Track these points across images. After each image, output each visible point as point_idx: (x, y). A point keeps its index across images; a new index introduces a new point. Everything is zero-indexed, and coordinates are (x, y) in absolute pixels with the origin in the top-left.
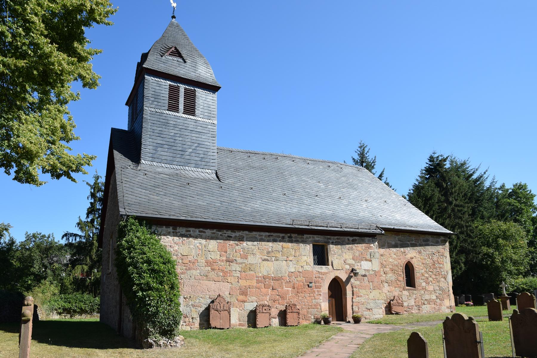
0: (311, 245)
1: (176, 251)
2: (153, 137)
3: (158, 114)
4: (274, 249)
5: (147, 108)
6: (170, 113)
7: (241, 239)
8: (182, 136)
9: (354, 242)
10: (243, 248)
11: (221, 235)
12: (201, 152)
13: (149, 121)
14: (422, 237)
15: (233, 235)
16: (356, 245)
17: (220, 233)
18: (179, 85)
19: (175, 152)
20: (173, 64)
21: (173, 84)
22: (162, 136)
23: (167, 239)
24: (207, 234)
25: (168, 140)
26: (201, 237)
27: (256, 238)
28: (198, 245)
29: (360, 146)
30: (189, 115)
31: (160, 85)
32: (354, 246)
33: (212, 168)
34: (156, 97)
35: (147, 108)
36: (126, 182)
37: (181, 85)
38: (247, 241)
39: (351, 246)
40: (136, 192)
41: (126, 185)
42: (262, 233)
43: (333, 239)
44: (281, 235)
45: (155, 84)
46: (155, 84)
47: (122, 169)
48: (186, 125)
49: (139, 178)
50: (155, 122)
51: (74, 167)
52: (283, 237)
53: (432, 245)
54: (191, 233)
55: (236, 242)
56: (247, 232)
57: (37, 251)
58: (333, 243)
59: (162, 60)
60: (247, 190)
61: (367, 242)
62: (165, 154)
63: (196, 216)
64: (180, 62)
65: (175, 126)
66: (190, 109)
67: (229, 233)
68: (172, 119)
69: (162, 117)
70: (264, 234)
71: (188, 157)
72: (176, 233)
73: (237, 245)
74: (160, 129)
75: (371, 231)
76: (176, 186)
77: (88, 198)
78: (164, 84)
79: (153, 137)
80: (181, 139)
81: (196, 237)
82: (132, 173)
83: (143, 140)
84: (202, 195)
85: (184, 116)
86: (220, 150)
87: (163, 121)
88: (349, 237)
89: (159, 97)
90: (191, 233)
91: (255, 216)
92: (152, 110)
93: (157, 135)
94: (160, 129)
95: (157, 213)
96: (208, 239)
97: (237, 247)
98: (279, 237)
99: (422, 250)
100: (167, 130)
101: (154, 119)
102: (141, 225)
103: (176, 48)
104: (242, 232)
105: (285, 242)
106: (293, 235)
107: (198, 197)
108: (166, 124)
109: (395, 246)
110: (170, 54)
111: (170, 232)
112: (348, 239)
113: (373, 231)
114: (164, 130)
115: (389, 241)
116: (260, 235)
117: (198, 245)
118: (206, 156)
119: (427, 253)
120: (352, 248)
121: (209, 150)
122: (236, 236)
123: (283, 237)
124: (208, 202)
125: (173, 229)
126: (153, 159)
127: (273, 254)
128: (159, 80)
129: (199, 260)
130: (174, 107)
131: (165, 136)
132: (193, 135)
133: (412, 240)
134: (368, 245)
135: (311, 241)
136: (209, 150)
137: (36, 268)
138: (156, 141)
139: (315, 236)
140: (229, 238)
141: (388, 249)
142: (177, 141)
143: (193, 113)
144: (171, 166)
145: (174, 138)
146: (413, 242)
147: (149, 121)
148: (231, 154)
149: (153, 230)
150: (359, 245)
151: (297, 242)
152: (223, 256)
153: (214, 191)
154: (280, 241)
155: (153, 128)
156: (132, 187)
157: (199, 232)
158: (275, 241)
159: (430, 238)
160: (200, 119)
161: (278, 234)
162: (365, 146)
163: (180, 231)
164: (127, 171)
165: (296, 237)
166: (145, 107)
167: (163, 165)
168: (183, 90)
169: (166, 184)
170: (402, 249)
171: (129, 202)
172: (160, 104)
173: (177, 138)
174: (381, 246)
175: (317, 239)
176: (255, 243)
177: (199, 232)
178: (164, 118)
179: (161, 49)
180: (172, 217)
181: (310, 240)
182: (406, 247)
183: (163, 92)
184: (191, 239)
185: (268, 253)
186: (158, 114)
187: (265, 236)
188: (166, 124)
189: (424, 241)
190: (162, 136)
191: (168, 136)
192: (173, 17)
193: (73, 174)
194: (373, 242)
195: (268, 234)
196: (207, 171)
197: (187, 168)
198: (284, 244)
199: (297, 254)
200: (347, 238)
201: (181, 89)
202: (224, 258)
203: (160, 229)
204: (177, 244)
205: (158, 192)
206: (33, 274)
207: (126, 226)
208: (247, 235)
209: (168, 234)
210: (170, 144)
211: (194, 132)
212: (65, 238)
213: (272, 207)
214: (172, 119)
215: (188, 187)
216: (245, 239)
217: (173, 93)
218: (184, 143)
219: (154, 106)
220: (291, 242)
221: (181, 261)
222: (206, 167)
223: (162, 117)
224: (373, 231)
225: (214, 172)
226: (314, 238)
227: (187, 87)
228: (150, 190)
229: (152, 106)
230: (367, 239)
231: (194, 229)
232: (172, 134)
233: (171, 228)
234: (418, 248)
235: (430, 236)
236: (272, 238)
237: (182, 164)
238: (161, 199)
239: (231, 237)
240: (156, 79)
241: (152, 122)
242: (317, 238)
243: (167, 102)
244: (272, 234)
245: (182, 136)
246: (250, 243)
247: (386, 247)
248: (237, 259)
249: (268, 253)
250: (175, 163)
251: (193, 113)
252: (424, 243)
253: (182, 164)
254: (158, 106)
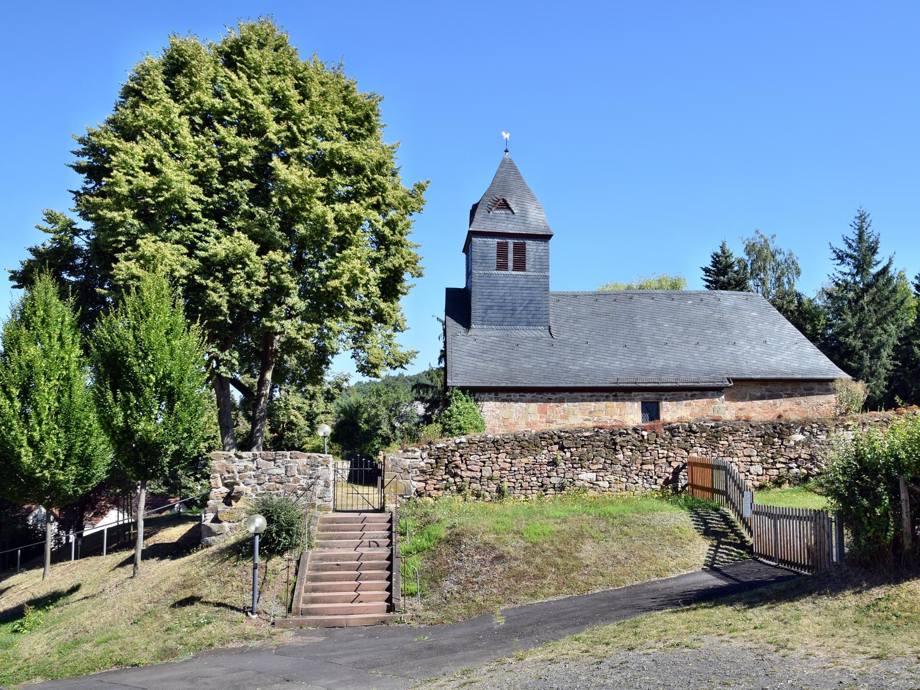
4: (596, 409)
5: (475, 272)
6: (499, 272)
7: (561, 401)
9: (693, 397)
10: (564, 410)
12: (532, 309)
14: (802, 386)
15: (554, 397)
16: (695, 400)
17: (540, 396)
19: (505, 312)
22: (491, 297)
25: (498, 301)
26: (522, 401)
32: (693, 402)
33: (545, 324)
35: (475, 272)
42: (584, 394)
44: (605, 394)
51: (404, 361)
53: (817, 394)
54: (512, 397)
56: (568, 394)
57: (384, 409)
58: (666, 400)
62: (496, 315)
65: (504, 285)
66: (520, 265)
67: (550, 395)
70: (585, 394)
71: (519, 316)
73: (558, 406)
74: (490, 291)
80: (511, 298)
81: (517, 401)
83: (472, 305)
85: (513, 273)
88: (687, 393)
90: (512, 397)
91: (579, 376)
92: (481, 272)
94: (490, 291)
99: (802, 401)
101: (482, 281)
102: (464, 394)
103: (504, 200)
105: (609, 401)
106: (619, 394)
107: (525, 359)
108: (495, 285)
109: (762, 398)
112: (686, 395)
116: (581, 396)
118: (537, 312)
120: (690, 405)
121: (541, 305)
123: (607, 397)
130: (502, 266)
131: (494, 297)
132: (523, 292)
133: (788, 390)
136: (541, 305)
137: (385, 429)
138: (485, 304)
139: (645, 393)
140: (549, 400)
146: (789, 392)
150: (699, 400)
151: (623, 400)
154: (604, 401)
155: (482, 291)
159: (816, 386)
160: (531, 274)
161: (602, 394)
162: (867, 214)
164: (458, 338)
165: (622, 396)
170: (771, 401)
173: (507, 298)
174: (727, 399)
183: (491, 251)
184: (512, 403)
185: (591, 412)
187: (587, 396)
189: (805, 390)
190: (491, 297)
191: (497, 297)
192: (506, 151)
194: (719, 396)
195: (590, 394)
198: (608, 403)
200: (684, 393)
201: (509, 245)
202: (544, 420)
203: (483, 396)
205: (485, 358)
206: (381, 436)
207: (451, 396)
209: (491, 400)
212: (415, 391)
213: (604, 363)
217: (502, 251)
218: (514, 301)
220: (617, 400)
222: (538, 324)
225: (547, 327)
229: (480, 268)
230: (710, 393)
232: (501, 294)
233: (493, 394)
235: (816, 384)
242: (647, 395)
243: (495, 261)
247: (747, 399)
250: (505, 323)
252: (805, 393)
254: (487, 268)
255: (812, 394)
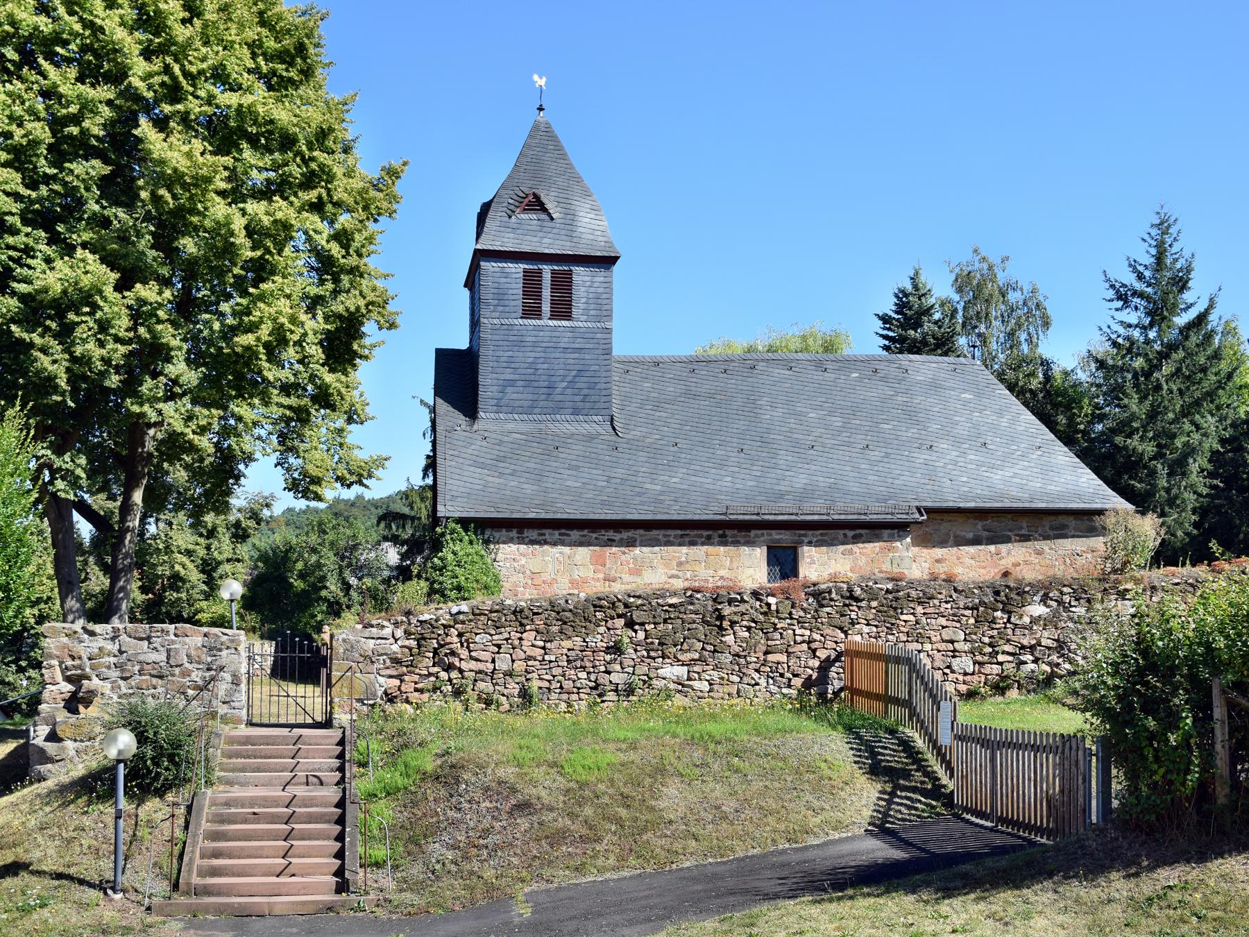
0: (765, 548)
1: (523, 566)
2: (498, 370)
3: (505, 327)
4: (690, 558)
5: (485, 321)
7: (631, 543)
8: (548, 361)
9: (856, 539)
10: (635, 559)
11: (596, 538)
13: (489, 342)
14: (1047, 522)
15: (617, 537)
16: (861, 545)
17: (594, 535)
18: (540, 267)
19: (537, 390)
20: (529, 227)
21: (531, 267)
23: (509, 549)
24: (573, 537)
25: (524, 371)
26: (563, 544)
27: (658, 540)
28: (557, 555)
29: (1158, 222)
30: (560, 320)
31: (507, 275)
32: (856, 548)
33: (603, 412)
34: (501, 297)
35: (485, 321)
36: (451, 458)
37: (545, 267)
38: (641, 545)
39: (849, 547)
40: (466, 473)
41: (451, 463)
42: (669, 532)
43: (813, 535)
44: (705, 533)
45: (499, 274)
46: (499, 274)
47: (448, 434)
48: (555, 339)
49: (473, 447)
50: (501, 343)
52: (709, 537)
53: (1073, 537)
55: (623, 549)
56: (641, 532)
58: (810, 543)
59: (510, 225)
60: (667, 448)
61: (885, 539)
62: (521, 396)
63: (554, 509)
64: (543, 220)
65: (535, 345)
66: (562, 309)
68: (529, 333)
69: (511, 333)
70: (672, 533)
71: (560, 398)
72: (523, 538)
73: (624, 553)
74: (510, 353)
75: (896, 518)
76: (535, 455)
77: (424, 434)
78: (514, 270)
79: (498, 370)
80: (546, 366)
81: (555, 544)
82: (463, 438)
83: (480, 378)
84: (577, 468)
85: (551, 323)
86: (634, 365)
87: (515, 338)
89: (506, 297)
91: (661, 502)
92: (495, 321)
93: (505, 365)
94: (510, 353)
95: (493, 510)
96: (575, 545)
97: (623, 557)
98: (701, 536)
99: (1046, 548)
100: (521, 354)
101: (497, 338)
102: (466, 530)
104: (633, 531)
106: (729, 532)
108: (519, 344)
109: (976, 541)
110: (525, 209)
111: (512, 538)
112: (845, 535)
113: (899, 516)
114: (517, 354)
115: (958, 533)
117: (557, 555)
118: (592, 392)
119: (1060, 552)
120: (851, 552)
122: (622, 539)
123: (709, 537)
124: (584, 480)
125: (518, 533)
126: (499, 408)
127: (688, 567)
128: (505, 265)
129: (559, 580)
130: (532, 311)
132: (568, 356)
133: (1021, 528)
134: (888, 544)
135: (764, 541)
136: (597, 380)
139: (773, 532)
140: (610, 543)
141: (955, 549)
142: (540, 372)
143: (567, 316)
144: (530, 416)
145: (534, 366)
146: (1023, 532)
147: (489, 342)
148: (657, 369)
149: (486, 537)
150: (866, 545)
151: (736, 543)
152: (599, 571)
153: (601, 457)
154: (703, 544)
155: (498, 354)
156: (460, 466)
157: (560, 534)
158: (692, 543)
159: (1071, 522)
160: (581, 324)
161: (700, 532)
163: (530, 535)
164: (456, 435)
165: (733, 536)
166: (482, 320)
167: (516, 416)
168: (549, 275)
169: (518, 452)
170: (992, 548)
171: (454, 493)
172: (507, 309)
173: (539, 366)
175: (778, 537)
176: (657, 549)
177: (560, 534)
178: (515, 333)
179: (511, 201)
180: (514, 516)
181: (762, 539)
182: (1003, 542)
183: (514, 286)
184: (546, 547)
185: (680, 564)
186: (505, 327)
187: (675, 536)
188: (519, 344)
189: (1052, 528)
190: (513, 365)
192: (541, 109)
193: (365, 481)
194: (901, 538)
195: (679, 532)
196: (595, 418)
197: (558, 416)
198: (710, 549)
199: (735, 565)
200: (841, 532)
201: (544, 275)
202: (601, 576)
203: (497, 535)
204: (524, 556)
207: (443, 535)
208: (641, 536)
209: (511, 540)
210: (528, 377)
211: (569, 350)
212: (382, 525)
214: (529, 333)
215: (556, 453)
216: (638, 543)
217: (531, 284)
218: (552, 372)
219: (497, 314)
220: (725, 544)
221: (530, 582)
222: (592, 412)
223: (511, 333)
224: (899, 516)
225: (608, 418)
226: (771, 535)
227: (556, 268)
228: (489, 467)
230: (886, 533)
231: (551, 531)
232: (530, 360)
233: (515, 531)
234: (1039, 545)
235: (1071, 518)
236: (687, 540)
237: (550, 411)
238: (505, 482)
239: (614, 541)
240: (500, 265)
241: (494, 343)
242: (776, 535)
243: (520, 303)
244: (688, 532)
245: (548, 361)
246: (645, 549)
247: (950, 544)
248: (623, 576)
249: (680, 564)
251: (567, 316)
252: (1051, 533)
253: (550, 411)
255: (1065, 536)
